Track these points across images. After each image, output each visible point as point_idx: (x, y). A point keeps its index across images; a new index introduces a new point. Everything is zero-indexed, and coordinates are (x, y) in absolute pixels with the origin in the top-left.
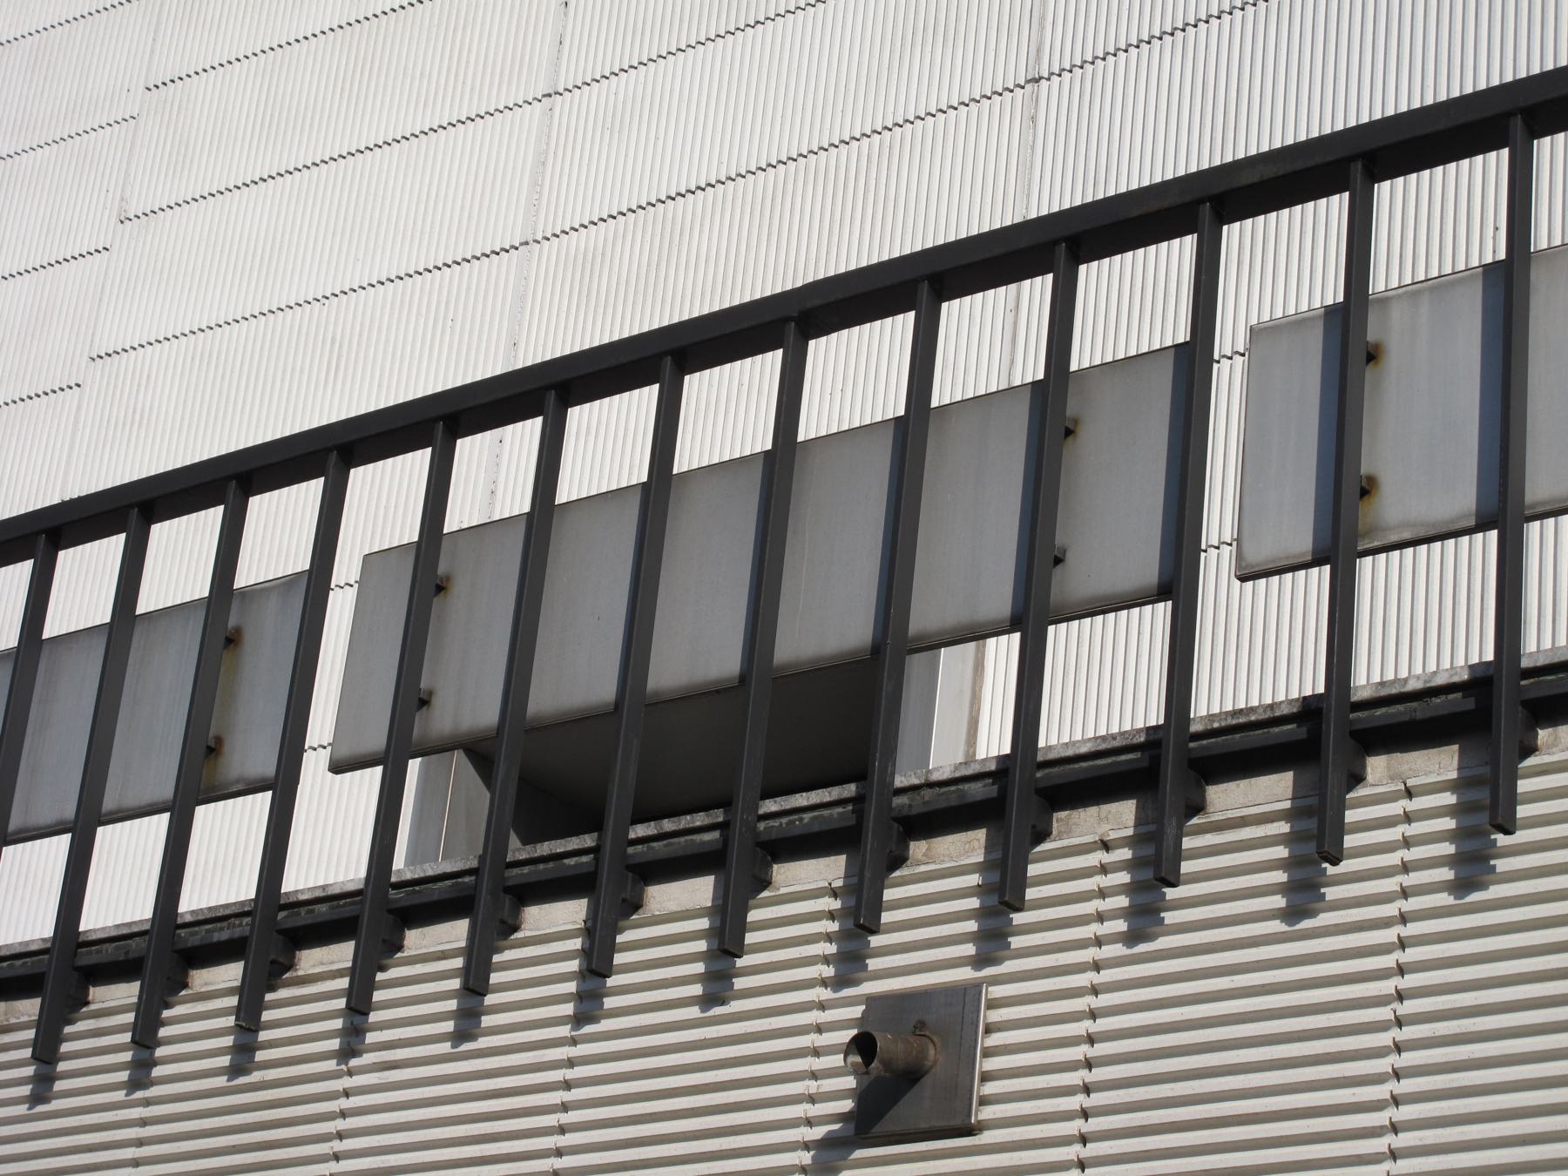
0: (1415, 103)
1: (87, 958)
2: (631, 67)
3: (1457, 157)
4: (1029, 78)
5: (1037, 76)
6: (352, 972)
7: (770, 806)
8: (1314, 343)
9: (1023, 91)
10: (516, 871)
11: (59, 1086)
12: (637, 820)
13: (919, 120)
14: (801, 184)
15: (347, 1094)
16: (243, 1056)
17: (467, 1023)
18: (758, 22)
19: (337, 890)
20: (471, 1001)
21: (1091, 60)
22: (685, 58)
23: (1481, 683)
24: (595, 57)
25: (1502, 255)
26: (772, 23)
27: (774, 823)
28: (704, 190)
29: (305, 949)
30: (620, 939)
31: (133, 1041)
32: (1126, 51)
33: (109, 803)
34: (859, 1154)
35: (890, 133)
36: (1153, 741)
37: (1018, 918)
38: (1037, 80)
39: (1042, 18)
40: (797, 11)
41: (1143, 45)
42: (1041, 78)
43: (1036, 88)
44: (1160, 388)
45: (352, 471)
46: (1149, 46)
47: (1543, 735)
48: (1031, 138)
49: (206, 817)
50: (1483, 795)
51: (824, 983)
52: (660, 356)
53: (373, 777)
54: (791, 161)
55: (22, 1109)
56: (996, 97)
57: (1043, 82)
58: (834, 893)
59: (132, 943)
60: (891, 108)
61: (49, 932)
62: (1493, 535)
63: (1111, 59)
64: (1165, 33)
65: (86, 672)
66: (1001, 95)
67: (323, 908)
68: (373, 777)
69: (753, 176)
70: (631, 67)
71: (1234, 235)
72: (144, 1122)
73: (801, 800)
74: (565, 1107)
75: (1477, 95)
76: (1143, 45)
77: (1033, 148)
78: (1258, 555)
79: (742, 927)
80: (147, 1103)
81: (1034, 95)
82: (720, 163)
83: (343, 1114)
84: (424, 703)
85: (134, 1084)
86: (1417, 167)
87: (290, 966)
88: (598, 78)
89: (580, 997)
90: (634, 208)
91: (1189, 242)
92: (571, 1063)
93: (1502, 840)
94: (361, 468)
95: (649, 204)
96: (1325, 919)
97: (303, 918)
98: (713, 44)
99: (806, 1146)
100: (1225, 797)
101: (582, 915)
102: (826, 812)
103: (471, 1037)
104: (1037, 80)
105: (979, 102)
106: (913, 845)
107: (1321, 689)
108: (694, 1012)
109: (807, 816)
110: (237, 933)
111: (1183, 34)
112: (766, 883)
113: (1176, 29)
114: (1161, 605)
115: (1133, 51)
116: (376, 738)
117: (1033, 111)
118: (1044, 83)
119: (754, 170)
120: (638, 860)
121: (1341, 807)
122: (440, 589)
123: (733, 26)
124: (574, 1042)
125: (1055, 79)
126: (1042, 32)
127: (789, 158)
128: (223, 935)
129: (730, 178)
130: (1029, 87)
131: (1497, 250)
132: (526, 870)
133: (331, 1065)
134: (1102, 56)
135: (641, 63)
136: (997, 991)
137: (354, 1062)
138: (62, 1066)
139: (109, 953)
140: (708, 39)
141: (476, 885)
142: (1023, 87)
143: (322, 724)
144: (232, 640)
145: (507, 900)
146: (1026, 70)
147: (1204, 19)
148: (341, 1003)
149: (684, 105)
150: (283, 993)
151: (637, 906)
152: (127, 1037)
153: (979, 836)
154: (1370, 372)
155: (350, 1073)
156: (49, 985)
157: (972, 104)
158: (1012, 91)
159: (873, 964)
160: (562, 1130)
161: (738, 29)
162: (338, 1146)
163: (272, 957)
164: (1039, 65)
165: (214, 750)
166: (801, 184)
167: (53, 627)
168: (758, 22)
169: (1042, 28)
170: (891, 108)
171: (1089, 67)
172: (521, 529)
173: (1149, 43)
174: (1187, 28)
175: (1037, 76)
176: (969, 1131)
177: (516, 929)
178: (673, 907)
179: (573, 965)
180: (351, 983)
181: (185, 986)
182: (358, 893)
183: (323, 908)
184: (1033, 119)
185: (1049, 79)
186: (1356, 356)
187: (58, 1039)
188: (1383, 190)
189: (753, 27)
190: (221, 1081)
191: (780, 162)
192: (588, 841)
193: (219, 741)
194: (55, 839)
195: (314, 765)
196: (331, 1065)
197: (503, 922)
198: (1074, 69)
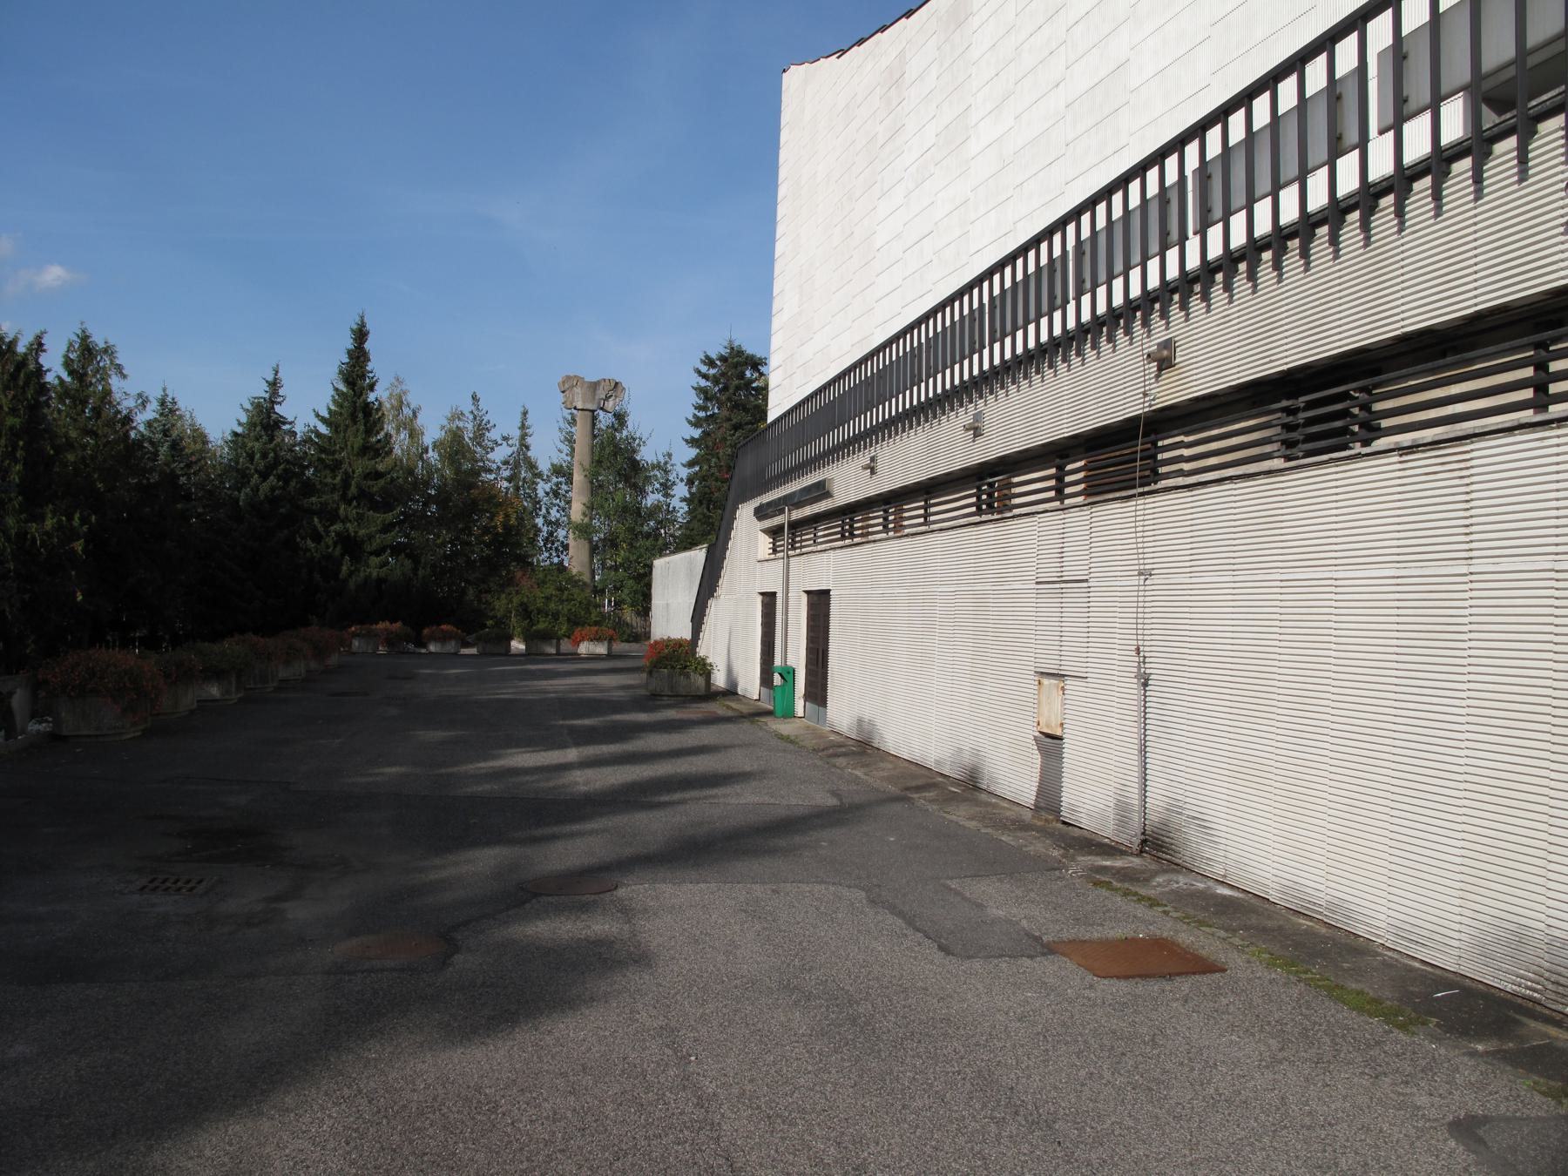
1: (1313, 220)
6: (1518, 149)
7: (1534, 103)
10: (1447, 152)
11: (1445, 208)
12: (1530, 99)
15: (1402, 245)
16: (1367, 241)
17: (1438, 210)
19: (1387, 176)
20: (1523, 167)
27: (1536, 109)
29: (1454, 163)
30: (1530, 148)
31: (1473, 182)
33: (1310, 166)
45: (1368, 25)
49: (1340, 162)
52: (1356, 21)
53: (1391, 134)
55: (1432, 221)
58: (1562, 129)
61: (1140, 293)
67: (1384, 183)
68: (1391, 134)
72: (1340, 270)
73: (1545, 97)
74: (1475, 232)
80: (1340, 263)
83: (1402, 252)
84: (1406, 101)
85: (1335, 258)
87: (1377, 206)
89: (1476, 191)
92: (1475, 216)
94: (1371, 22)
97: (1379, 188)
101: (1471, 163)
102: (1555, 99)
106: (1263, 254)
108: (1516, 187)
109: (1548, 103)
110: (1391, 183)
112: (1536, 132)
116: (1390, 120)
120: (1535, 114)
122: (1405, 57)
124: (1475, 208)
128: (1352, 201)
132: (1450, 151)
133: (1396, 236)
137: (1403, 234)
138: (1444, 201)
141: (1472, 143)
144: (1339, 98)
145: (1444, 164)
148: (1516, 162)
150: (1376, 216)
151: (1490, 153)
152: (1470, 181)
154: (1405, 62)
155: (1403, 238)
156: (1300, 233)
160: (1475, 240)
162: (1402, 263)
163: (1369, 205)
165: (1339, 138)
167: (1309, 93)
172: (1296, 112)
176: (1174, 366)
177: (1449, 173)
178: (1503, 150)
180: (1566, 133)
181: (1345, 221)
182: (1270, 236)
187: (1527, 152)
190: (1432, 221)
192: (1514, 112)
193: (1341, 134)
194: (1265, 200)
196: (1396, 236)
197: (1443, 172)
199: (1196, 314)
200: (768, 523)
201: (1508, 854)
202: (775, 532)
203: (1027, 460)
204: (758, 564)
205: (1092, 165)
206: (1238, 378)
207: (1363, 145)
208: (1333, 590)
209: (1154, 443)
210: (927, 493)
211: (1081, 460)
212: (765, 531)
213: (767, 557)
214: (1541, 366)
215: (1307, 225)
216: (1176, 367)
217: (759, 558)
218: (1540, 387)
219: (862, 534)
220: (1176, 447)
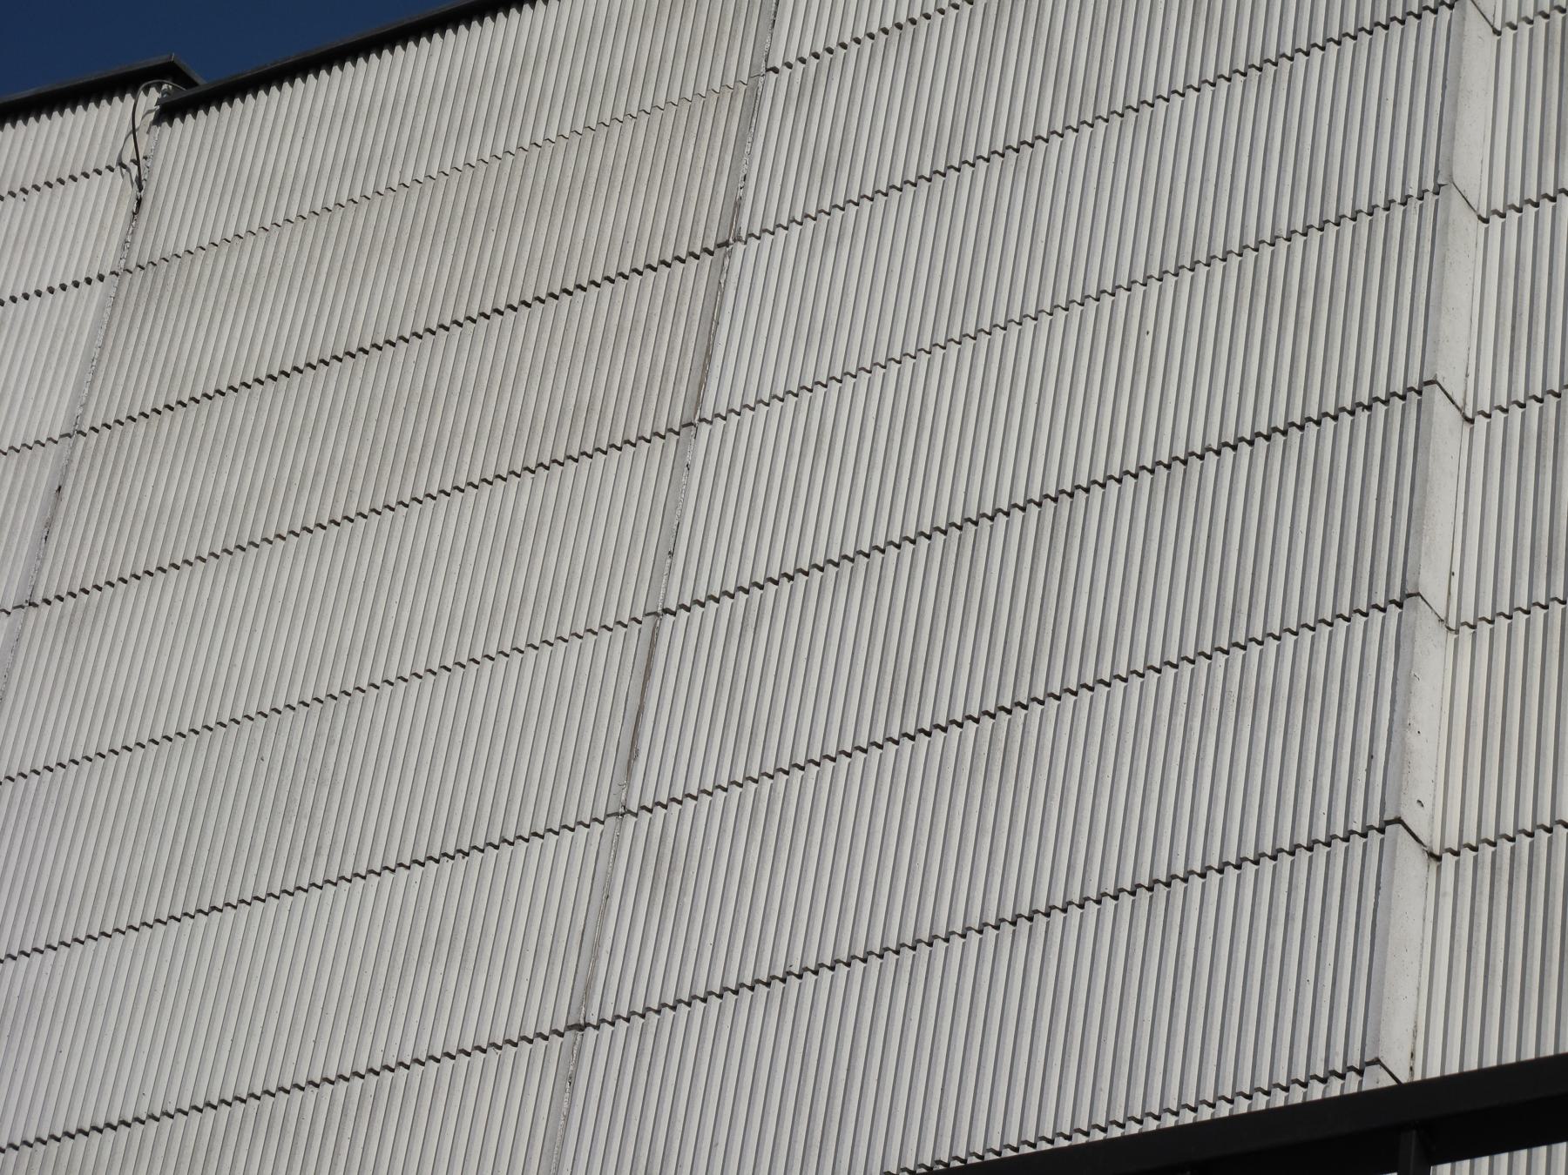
0: (1352, 1086)
2: (36, 950)
3: (1530, 1142)
4: (570, 1024)
5: (582, 1022)
9: (561, 1039)
13: (417, 1065)
14: (248, 1135)
18: (214, 908)
21: (656, 1008)
22: (110, 947)
24: (14, 926)
26: (234, 911)
28: (87, 1134)
32: (848, 965)
35: (376, 1078)
38: (581, 1027)
39: (597, 945)
40: (296, 892)
41: (728, 995)
42: (587, 1025)
43: (579, 1038)
46: (799, 981)
48: (566, 1105)
54: (238, 1102)
56: (524, 1044)
57: (590, 1030)
60: (381, 1045)
63: (683, 1009)
64: (758, 981)
66: (531, 1041)
69: (185, 1117)
70: (36, 950)
75: (1521, 1067)
76: (728, 995)
77: (567, 1118)
81: (576, 1048)
82: (141, 1094)
88: (15, 954)
90: (45, 1138)
95: (38, 1140)
98: (150, 930)
104: (581, 1027)
105: (500, 1048)
111: (782, 985)
113: (774, 977)
115: (714, 1001)
117: (571, 1068)
118: (591, 1033)
119: (186, 1109)
123: (31, 944)
125: (607, 1028)
126: (595, 961)
127: (236, 1098)
129: (124, 1123)
130: (569, 1035)
134: (749, 984)
135: (49, 946)
140: (117, 930)
142: (561, 1035)
146: (569, 1013)
147: (877, 952)
149: (101, 1010)
157: (491, 1050)
158: (546, 1038)
161: (186, 914)
164: (586, 1009)
166: (248, 1135)
168: (214, 908)
169: (595, 957)
170: (381, 1045)
171: (653, 1017)
173: (736, 992)
174: (869, 957)
175: (582, 1022)
184: (572, 1080)
185: (597, 1027)
189: (207, 914)
191: (223, 1101)
198: (725, 994)
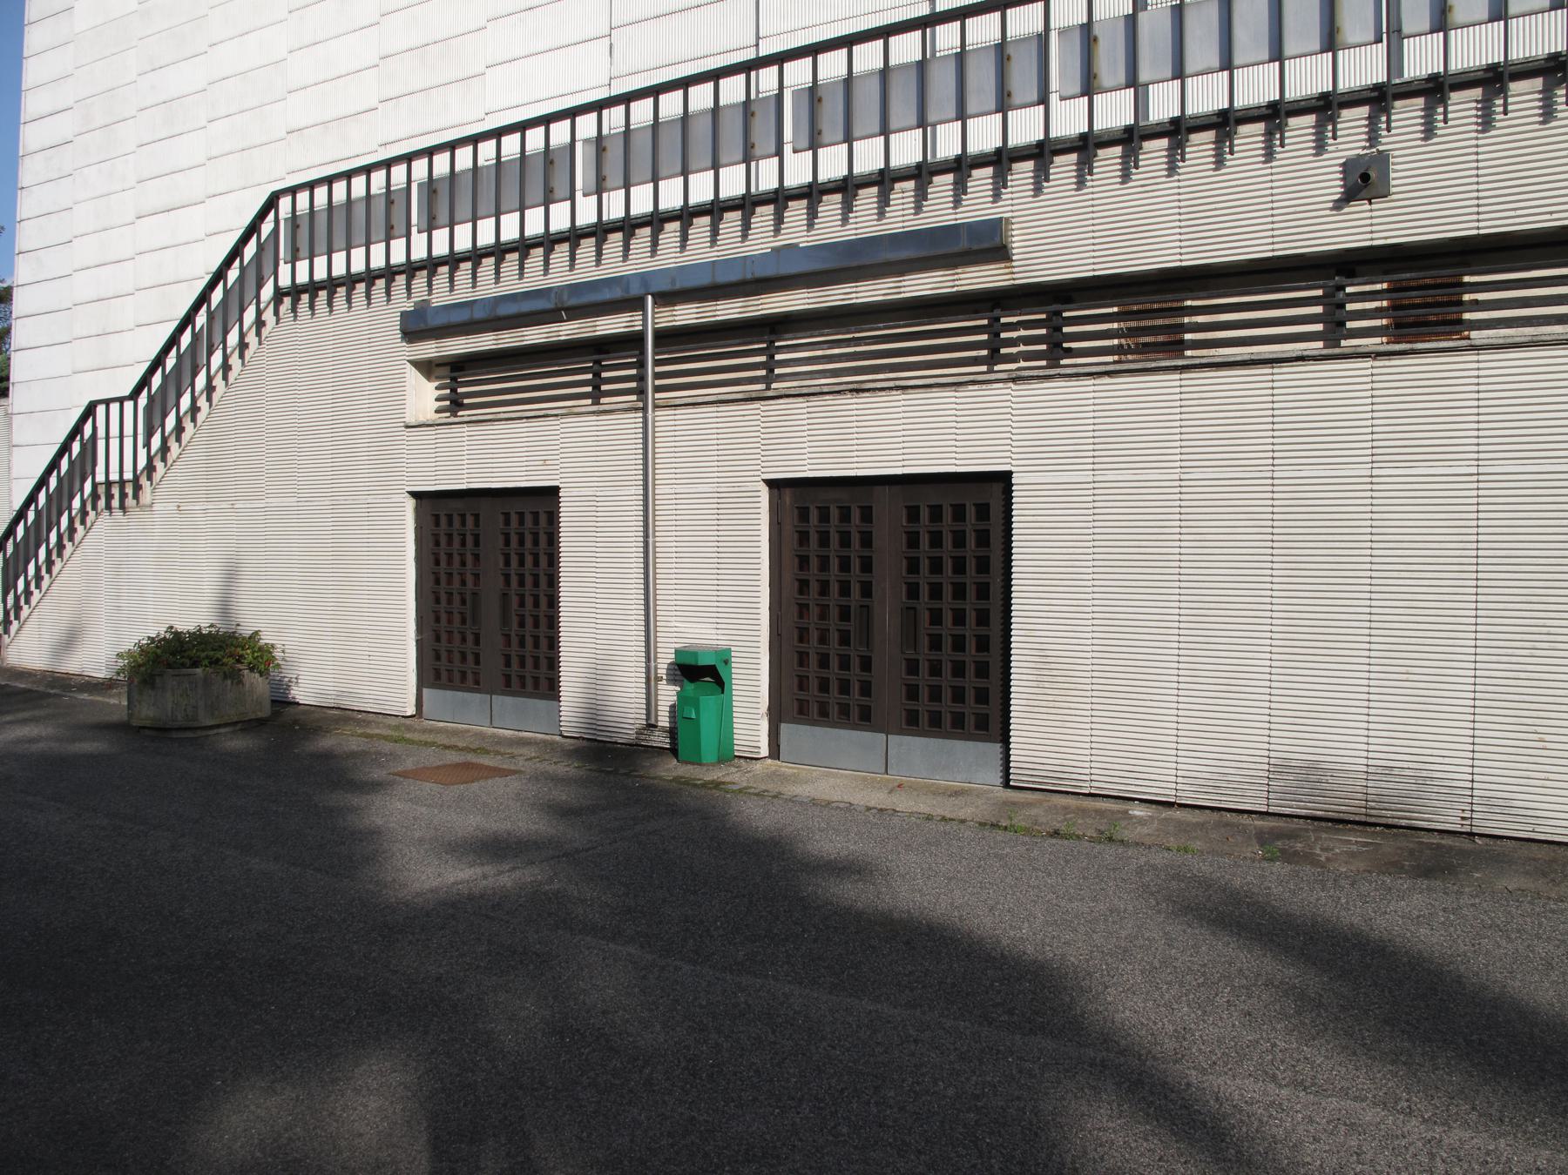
8: (992, 55)
23: (998, 151)
25: (1131, 12)
34: (1352, 203)
36: (810, 186)
37: (816, 221)
44: (1034, 47)
47: (694, 220)
50: (920, 193)
51: (1477, 131)
59: (1250, 111)
62: (1132, 89)
65: (875, 86)
71: (892, 40)
78: (1065, 94)
79: (688, 235)
85: (496, 283)
86: (864, 42)
91: (569, 121)
93: (964, 197)
96: (1435, 140)
99: (1394, 193)
100: (976, 173)
103: (1271, 161)
107: (1132, 122)
108: (1537, 126)
114: (1175, 81)
116: (593, 187)
121: (1093, 162)
131: (1085, 20)
136: (1396, 153)
139: (1346, 98)
143: (1054, 84)
153: (740, 213)
154: (604, 154)
159: (782, 232)
179: (805, 222)
182: (403, 265)
183: (1303, 103)
186: (749, 115)
188: (1009, 11)
195: (579, 195)
199: (634, 256)
200: (430, 349)
201: (1245, 613)
202: (452, 371)
203: (477, 360)
204: (407, 432)
205: (319, 122)
206: (1386, 238)
207: (408, 236)
208: (674, 476)
209: (1059, 313)
210: (600, 352)
211: (1382, 282)
212: (427, 368)
213: (431, 416)
214: (597, 375)
215: (331, 284)
216: (1389, 198)
217: (411, 420)
218: (770, 366)
219: (1121, 346)
220: (1200, 312)
